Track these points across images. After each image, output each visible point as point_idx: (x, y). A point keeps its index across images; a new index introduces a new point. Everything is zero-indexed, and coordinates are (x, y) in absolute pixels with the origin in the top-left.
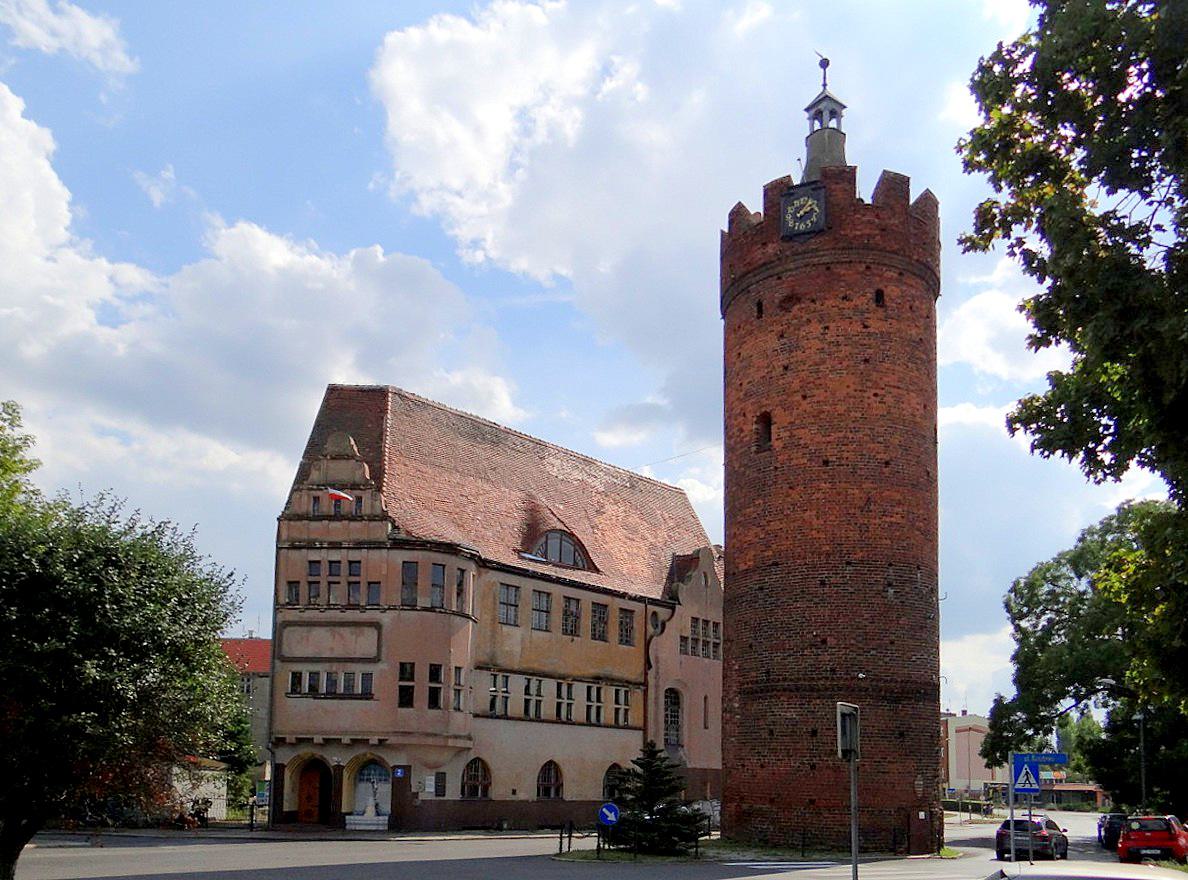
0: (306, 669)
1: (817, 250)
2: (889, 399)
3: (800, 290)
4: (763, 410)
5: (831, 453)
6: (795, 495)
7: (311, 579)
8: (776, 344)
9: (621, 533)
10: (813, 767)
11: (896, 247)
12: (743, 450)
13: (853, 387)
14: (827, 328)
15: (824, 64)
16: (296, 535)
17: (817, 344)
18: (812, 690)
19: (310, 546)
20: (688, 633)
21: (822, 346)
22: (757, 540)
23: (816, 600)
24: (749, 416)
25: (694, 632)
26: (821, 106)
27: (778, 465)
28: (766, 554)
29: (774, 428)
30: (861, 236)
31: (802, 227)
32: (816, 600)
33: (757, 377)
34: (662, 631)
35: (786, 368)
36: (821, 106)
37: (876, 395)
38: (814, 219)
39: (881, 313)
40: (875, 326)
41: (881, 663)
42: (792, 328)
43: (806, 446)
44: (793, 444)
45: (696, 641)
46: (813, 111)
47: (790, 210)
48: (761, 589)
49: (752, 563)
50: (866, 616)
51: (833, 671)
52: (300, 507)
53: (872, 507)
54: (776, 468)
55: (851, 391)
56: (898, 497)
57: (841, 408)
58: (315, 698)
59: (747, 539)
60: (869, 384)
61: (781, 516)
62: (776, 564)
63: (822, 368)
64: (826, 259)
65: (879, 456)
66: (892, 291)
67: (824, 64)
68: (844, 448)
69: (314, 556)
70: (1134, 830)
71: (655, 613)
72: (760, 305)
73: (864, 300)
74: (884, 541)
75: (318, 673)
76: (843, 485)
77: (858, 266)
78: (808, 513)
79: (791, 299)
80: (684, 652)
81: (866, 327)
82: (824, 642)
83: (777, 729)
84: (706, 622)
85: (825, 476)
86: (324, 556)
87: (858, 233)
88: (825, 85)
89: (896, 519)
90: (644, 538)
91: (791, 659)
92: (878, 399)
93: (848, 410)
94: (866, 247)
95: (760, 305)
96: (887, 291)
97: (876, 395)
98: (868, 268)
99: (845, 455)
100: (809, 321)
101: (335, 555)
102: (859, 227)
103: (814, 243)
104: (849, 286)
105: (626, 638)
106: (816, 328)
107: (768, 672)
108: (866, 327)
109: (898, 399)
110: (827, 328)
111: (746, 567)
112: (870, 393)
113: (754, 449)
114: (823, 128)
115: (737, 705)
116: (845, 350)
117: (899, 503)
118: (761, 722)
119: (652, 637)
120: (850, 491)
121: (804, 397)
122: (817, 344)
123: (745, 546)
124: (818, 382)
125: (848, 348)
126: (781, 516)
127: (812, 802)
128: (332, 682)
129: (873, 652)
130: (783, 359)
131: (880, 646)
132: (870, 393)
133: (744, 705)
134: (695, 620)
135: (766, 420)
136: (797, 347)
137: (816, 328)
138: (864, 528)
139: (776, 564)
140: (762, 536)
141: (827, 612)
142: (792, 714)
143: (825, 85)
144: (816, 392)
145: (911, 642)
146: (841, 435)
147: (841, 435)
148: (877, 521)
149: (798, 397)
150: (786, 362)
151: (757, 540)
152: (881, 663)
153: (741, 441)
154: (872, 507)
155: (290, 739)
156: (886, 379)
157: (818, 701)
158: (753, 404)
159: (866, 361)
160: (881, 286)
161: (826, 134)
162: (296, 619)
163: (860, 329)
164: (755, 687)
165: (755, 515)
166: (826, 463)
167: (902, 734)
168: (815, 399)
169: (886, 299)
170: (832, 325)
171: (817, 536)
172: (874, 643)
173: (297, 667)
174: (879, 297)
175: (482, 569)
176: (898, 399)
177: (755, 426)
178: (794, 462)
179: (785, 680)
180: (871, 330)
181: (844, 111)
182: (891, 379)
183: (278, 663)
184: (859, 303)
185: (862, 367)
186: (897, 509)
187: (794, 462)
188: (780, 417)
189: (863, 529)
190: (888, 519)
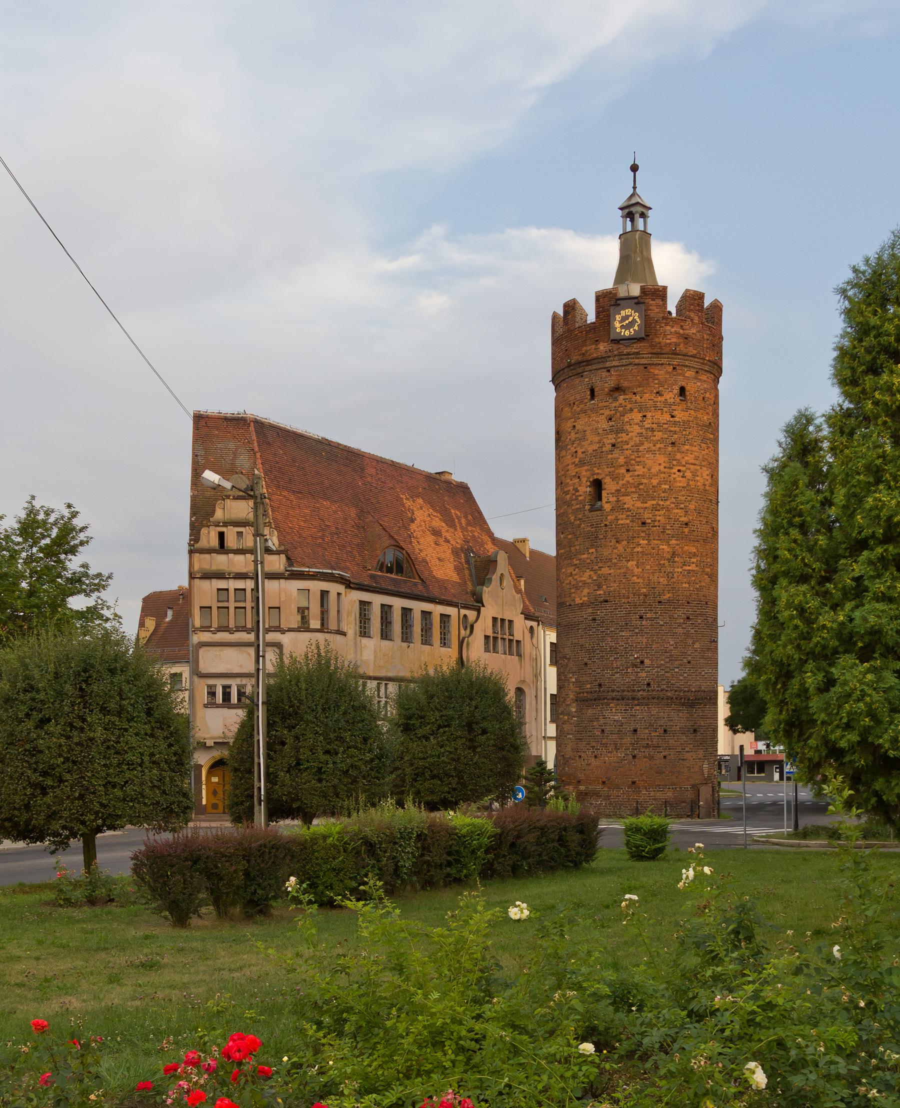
0: (219, 684)
1: (638, 353)
2: (688, 474)
3: (625, 384)
4: (595, 477)
5: (647, 516)
6: (620, 547)
7: (221, 605)
8: (605, 425)
9: (431, 538)
10: (634, 757)
11: (695, 352)
12: (578, 506)
13: (664, 465)
14: (645, 416)
15: (634, 168)
16: (206, 566)
17: (637, 429)
18: (633, 699)
19: (220, 576)
20: (490, 633)
21: (641, 431)
22: (590, 581)
23: (637, 631)
24: (584, 480)
25: (494, 632)
26: (633, 209)
27: (607, 523)
28: (599, 592)
29: (604, 494)
30: (670, 344)
31: (627, 333)
32: (637, 631)
33: (590, 449)
34: (471, 632)
35: (614, 445)
36: (633, 209)
37: (679, 471)
38: (636, 328)
39: (683, 405)
40: (680, 416)
41: (681, 678)
42: (618, 414)
43: (629, 510)
44: (619, 507)
45: (495, 638)
46: (627, 211)
47: (618, 318)
48: (594, 619)
49: (586, 599)
50: (672, 643)
51: (649, 684)
52: (209, 542)
53: (676, 559)
54: (606, 525)
55: (662, 468)
56: (694, 550)
57: (655, 482)
58: (229, 708)
59: (582, 579)
60: (675, 462)
61: (609, 564)
62: (606, 601)
63: (641, 448)
64: (643, 361)
65: (681, 519)
66: (690, 388)
67: (634, 168)
68: (657, 513)
69: (222, 584)
70: (507, 913)
71: (465, 616)
72: (592, 391)
73: (671, 396)
74: (684, 585)
75: (229, 687)
76: (656, 542)
77: (668, 367)
78: (630, 563)
79: (618, 389)
80: (487, 650)
81: (672, 417)
82: (642, 662)
83: (608, 729)
84: (503, 620)
85: (643, 534)
86: (233, 585)
87: (668, 341)
88: (635, 188)
89: (693, 567)
90: (447, 541)
91: (617, 675)
92: (681, 474)
93: (660, 483)
94: (675, 353)
95: (592, 391)
96: (688, 388)
97: (679, 471)
98: (674, 368)
99: (658, 518)
100: (631, 410)
101: (240, 584)
102: (669, 337)
103: (635, 348)
104: (661, 384)
105: (444, 642)
106: (637, 416)
107: (600, 685)
108: (672, 417)
109: (695, 475)
110: (645, 416)
111: (581, 602)
112: (675, 470)
113: (587, 507)
114: (634, 230)
115: (574, 710)
116: (658, 435)
117: (695, 555)
118: (595, 723)
119: (464, 638)
120: (661, 547)
121: (628, 470)
122: (637, 429)
123: (580, 584)
124: (638, 459)
125: (660, 433)
126: (609, 564)
127: (634, 783)
128: (227, 696)
129: (676, 670)
130: (611, 439)
131: (681, 665)
132: (675, 470)
133: (580, 710)
134: (495, 619)
135: (598, 485)
136: (623, 431)
137: (637, 416)
138: (670, 575)
139: (606, 601)
140: (595, 578)
141: (645, 640)
142: (618, 717)
143: (635, 188)
144: (637, 468)
145: (702, 661)
146: (654, 502)
147: (654, 502)
148: (680, 570)
149: (623, 471)
150: (614, 441)
151: (590, 581)
152: (681, 678)
153: (576, 499)
154: (676, 559)
155: (210, 743)
156: (686, 458)
157: (638, 708)
158: (586, 471)
159: (673, 443)
160: (683, 384)
161: (637, 237)
162: (210, 640)
163: (668, 418)
164: (589, 696)
165: (588, 561)
166: (644, 523)
167: (695, 731)
168: (636, 473)
169: (687, 393)
170: (649, 415)
171: (638, 581)
172: (677, 662)
173: (211, 682)
174: (682, 391)
175: (349, 590)
176: (695, 475)
177: (588, 489)
178: (620, 522)
179: (613, 691)
180: (677, 419)
181: (650, 213)
182: (690, 458)
183: (196, 678)
184: (668, 397)
185: (670, 449)
186: (693, 560)
187: (620, 522)
188: (609, 485)
189: (670, 576)
190: (687, 568)
